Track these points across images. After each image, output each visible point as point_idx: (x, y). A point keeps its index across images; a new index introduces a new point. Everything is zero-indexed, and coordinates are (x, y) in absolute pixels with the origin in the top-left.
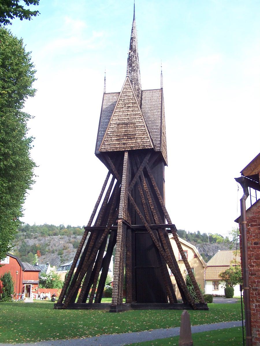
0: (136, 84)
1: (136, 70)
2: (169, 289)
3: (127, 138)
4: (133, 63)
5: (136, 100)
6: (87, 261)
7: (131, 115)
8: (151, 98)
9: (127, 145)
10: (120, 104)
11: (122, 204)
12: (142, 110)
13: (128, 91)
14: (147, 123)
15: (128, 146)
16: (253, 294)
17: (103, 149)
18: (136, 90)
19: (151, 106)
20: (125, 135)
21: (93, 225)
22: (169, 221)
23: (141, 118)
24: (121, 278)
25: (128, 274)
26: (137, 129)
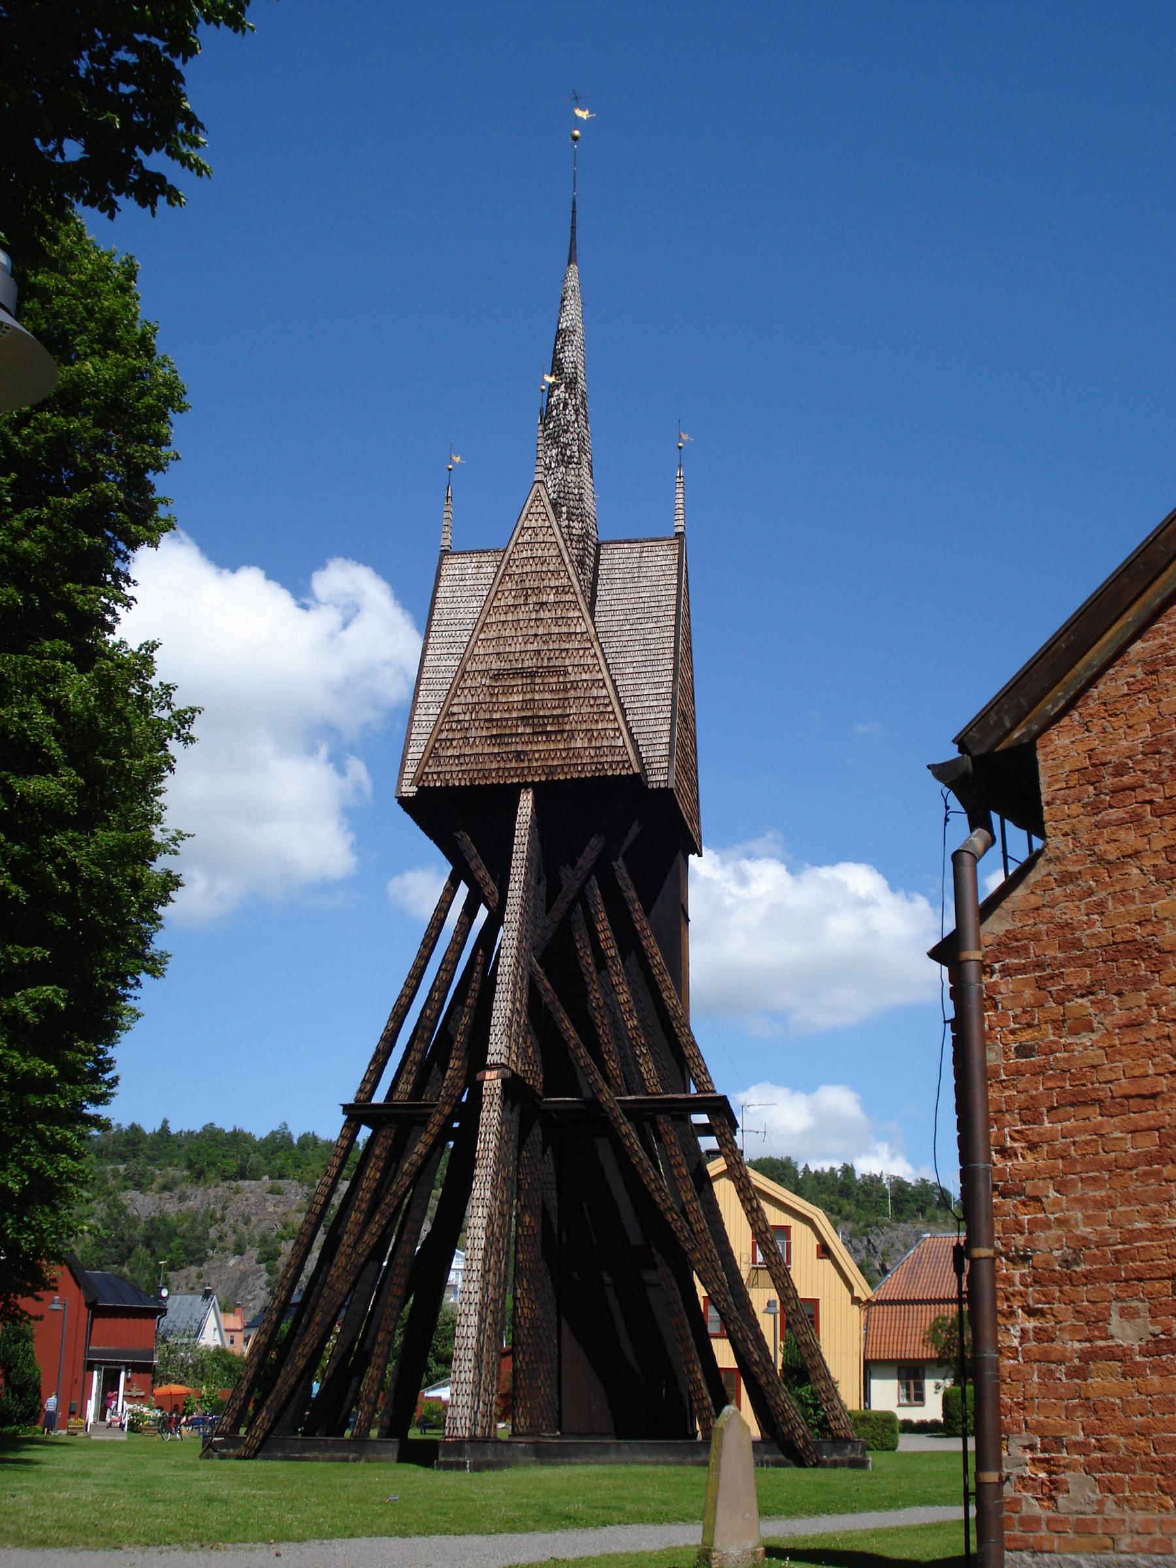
0: (575, 517)
1: (575, 460)
2: (699, 1377)
3: (534, 733)
4: (566, 431)
5: (574, 579)
6: (349, 1250)
7: (548, 637)
8: (636, 575)
9: (529, 760)
10: (506, 594)
11: (503, 1006)
12: (596, 619)
13: (540, 538)
14: (618, 671)
15: (535, 764)
16: (1009, 1280)
17: (430, 776)
18: (575, 538)
19: (636, 606)
20: (523, 718)
21: (379, 1097)
22: (704, 1084)
23: (592, 652)
24: (489, 1320)
25: (525, 1310)
26: (572, 693)
